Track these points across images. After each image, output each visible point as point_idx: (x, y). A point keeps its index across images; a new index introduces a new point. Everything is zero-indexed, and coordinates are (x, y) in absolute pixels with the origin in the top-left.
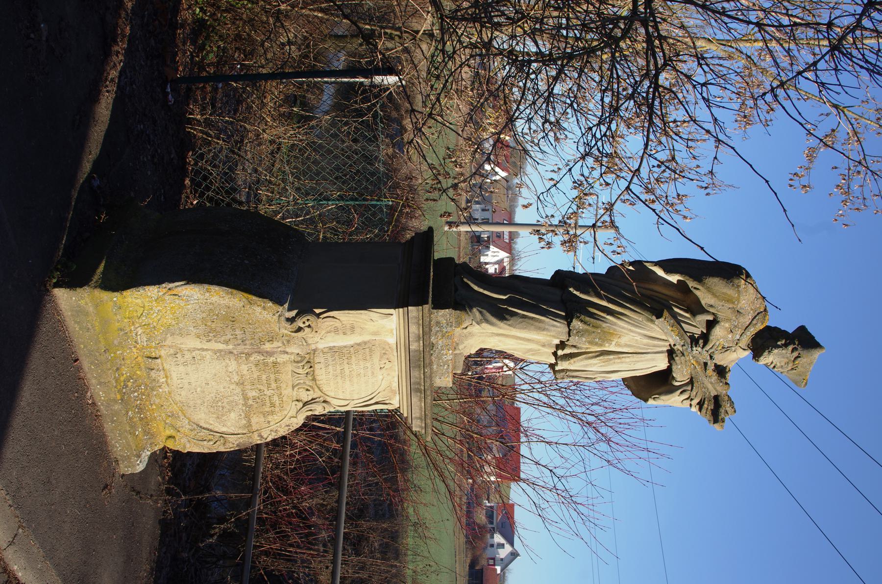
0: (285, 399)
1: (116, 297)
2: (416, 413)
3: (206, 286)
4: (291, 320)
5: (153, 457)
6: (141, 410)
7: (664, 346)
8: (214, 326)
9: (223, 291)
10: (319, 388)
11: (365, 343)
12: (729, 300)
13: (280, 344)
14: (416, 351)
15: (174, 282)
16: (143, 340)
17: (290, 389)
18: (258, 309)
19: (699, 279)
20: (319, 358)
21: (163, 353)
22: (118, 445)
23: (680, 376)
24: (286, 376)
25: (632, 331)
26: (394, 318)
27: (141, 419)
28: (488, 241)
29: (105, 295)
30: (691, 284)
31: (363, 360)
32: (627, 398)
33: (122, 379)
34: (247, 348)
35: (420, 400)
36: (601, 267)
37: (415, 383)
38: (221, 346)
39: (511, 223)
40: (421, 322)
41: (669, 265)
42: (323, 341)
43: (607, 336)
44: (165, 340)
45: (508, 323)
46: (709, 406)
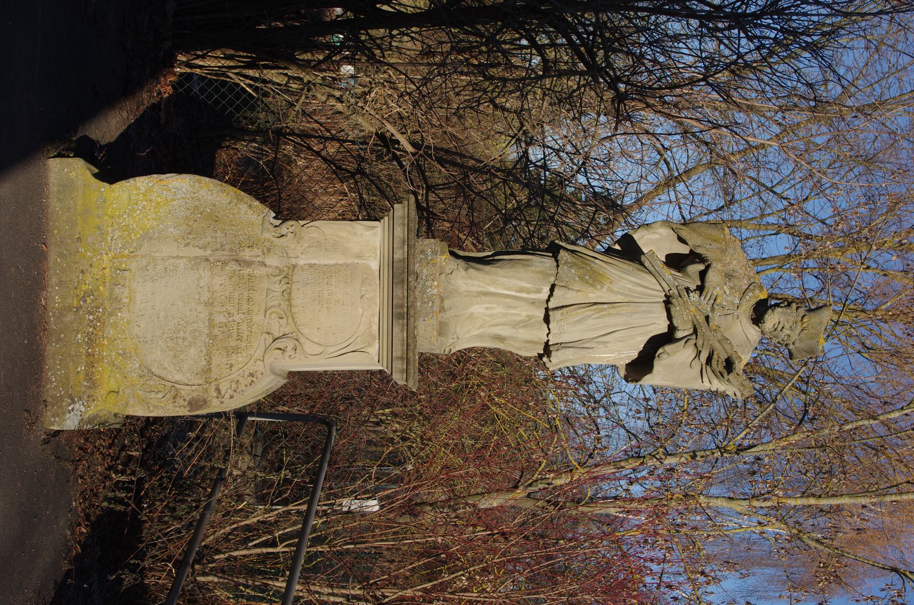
3: (197, 177)
6: (91, 341)
7: (660, 297)
10: (293, 319)
13: (259, 252)
14: (400, 261)
17: (262, 316)
18: (244, 208)
20: (298, 276)
21: (133, 265)
25: (624, 279)
35: (402, 330)
37: (397, 306)
40: (406, 221)
42: (303, 256)
44: (141, 246)
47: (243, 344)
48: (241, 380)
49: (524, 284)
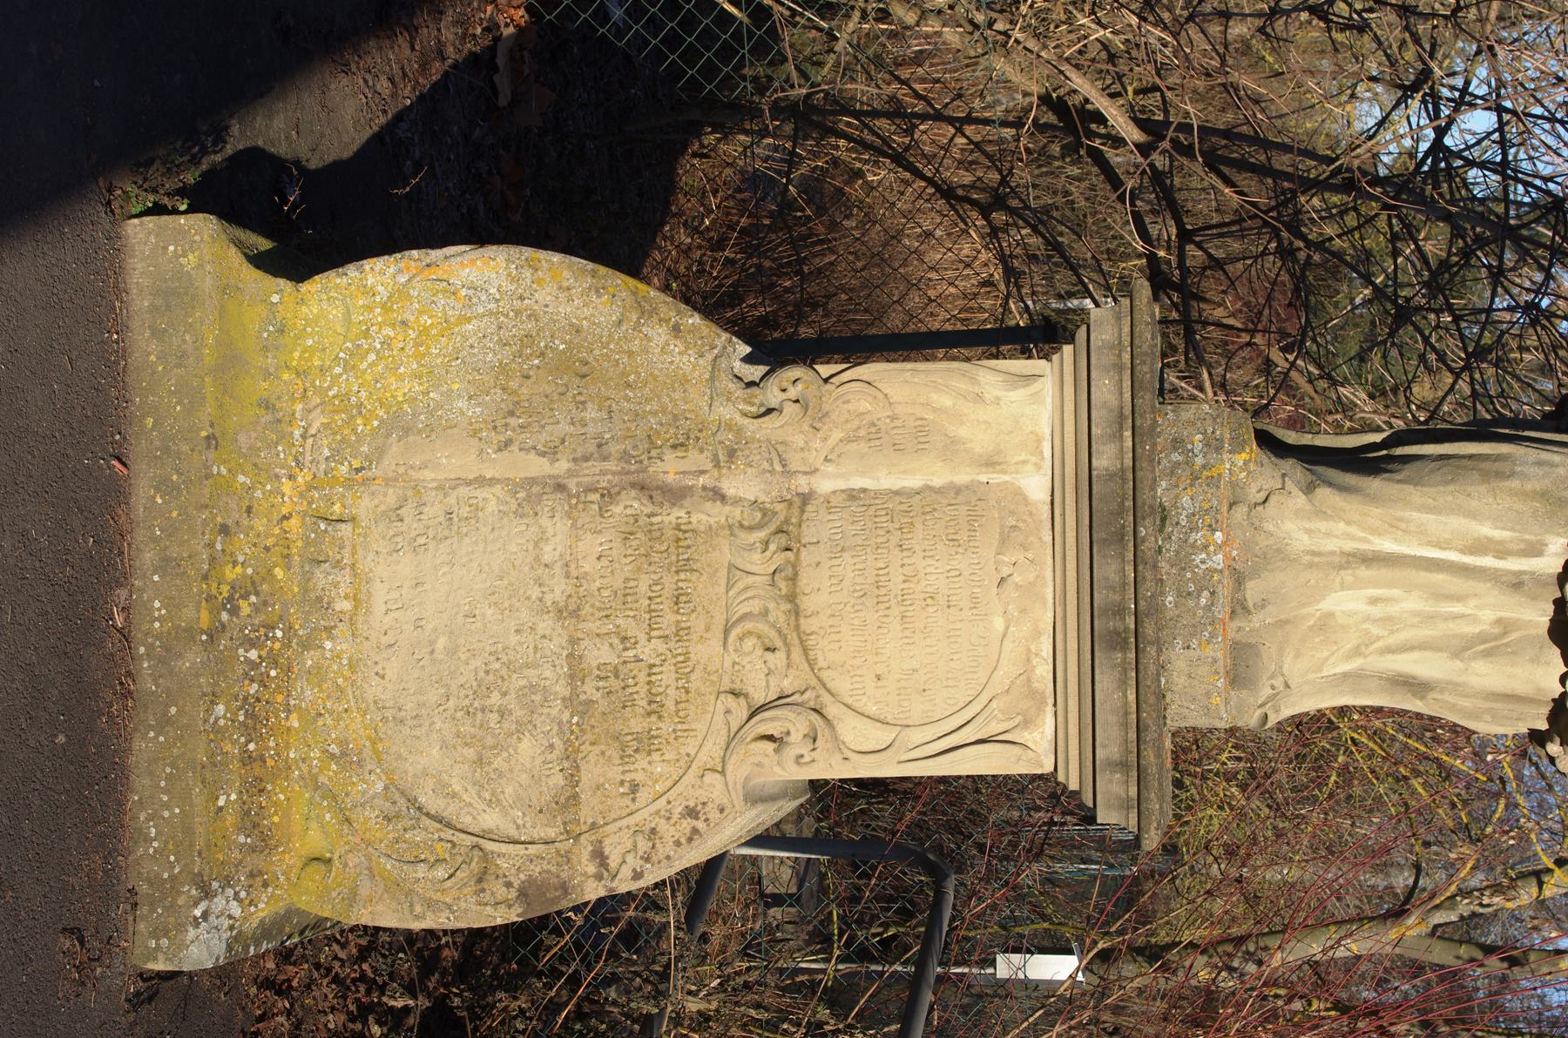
0: (695, 682)
1: (279, 290)
3: (528, 252)
6: (254, 721)
9: (570, 267)
11: (958, 490)
15: (442, 247)
17: (715, 643)
18: (659, 334)
20: (817, 528)
21: (364, 506)
22: (165, 808)
26: (1047, 387)
27: (247, 759)
33: (231, 573)
35: (1123, 683)
37: (1105, 611)
38: (538, 466)
42: (830, 468)
45: (1397, 476)
47: (666, 727)
48: (663, 827)
49: (1486, 530)
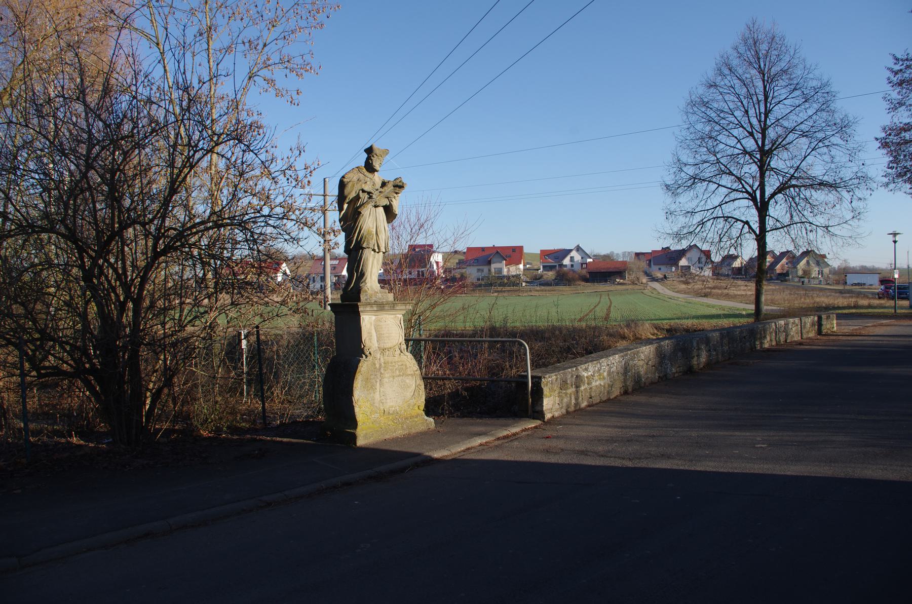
2: (403, 307)
4: (366, 356)
5: (428, 414)
6: (407, 418)
8: (369, 386)
12: (353, 185)
16: (377, 415)
19: (346, 197)
20: (382, 346)
22: (422, 428)
23: (386, 202)
24: (390, 359)
28: (339, 277)
29: (359, 428)
30: (347, 200)
31: (383, 328)
32: (396, 222)
34: (379, 374)
36: (343, 234)
39: (323, 258)
41: (341, 209)
43: (370, 233)
46: (397, 190)
